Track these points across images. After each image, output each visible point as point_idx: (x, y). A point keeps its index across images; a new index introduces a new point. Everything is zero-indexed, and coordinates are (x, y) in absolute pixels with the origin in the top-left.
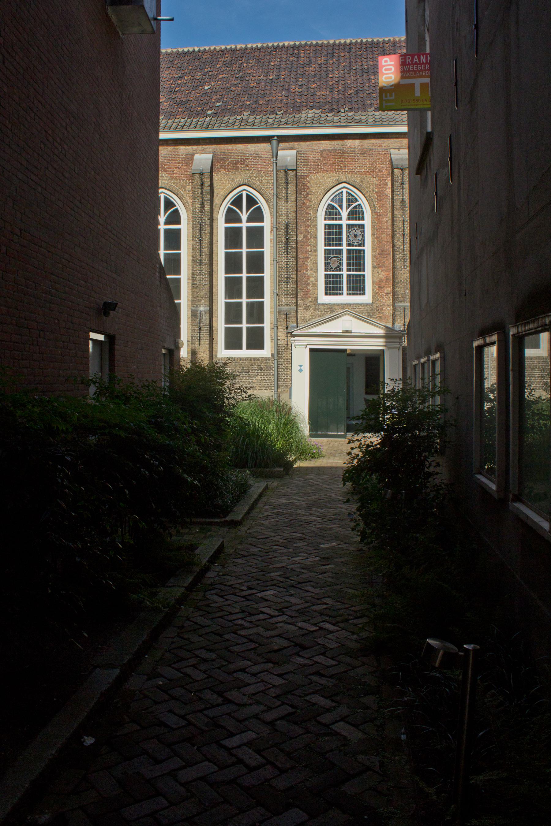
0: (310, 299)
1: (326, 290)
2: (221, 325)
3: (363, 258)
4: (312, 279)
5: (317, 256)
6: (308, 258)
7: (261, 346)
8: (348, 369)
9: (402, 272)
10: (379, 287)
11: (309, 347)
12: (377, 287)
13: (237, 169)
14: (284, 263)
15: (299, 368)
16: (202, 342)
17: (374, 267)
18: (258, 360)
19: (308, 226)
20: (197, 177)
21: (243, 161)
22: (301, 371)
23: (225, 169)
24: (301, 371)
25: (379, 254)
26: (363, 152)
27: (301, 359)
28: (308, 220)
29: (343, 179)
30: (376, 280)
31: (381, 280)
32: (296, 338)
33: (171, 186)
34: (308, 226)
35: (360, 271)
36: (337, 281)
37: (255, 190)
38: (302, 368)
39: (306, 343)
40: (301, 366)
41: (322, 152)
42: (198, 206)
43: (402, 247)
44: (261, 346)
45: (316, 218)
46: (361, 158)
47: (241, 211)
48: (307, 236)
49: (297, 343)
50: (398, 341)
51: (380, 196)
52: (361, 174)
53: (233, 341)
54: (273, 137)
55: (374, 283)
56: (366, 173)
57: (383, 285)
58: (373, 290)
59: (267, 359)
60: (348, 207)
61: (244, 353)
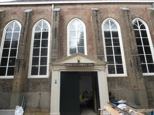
0: (64, 56)
1: (70, 53)
2: (30, 66)
3: (84, 49)
4: (65, 49)
5: (67, 41)
6: (63, 41)
7: (122, 72)
8: (70, 42)
9: (99, 44)
10: (90, 51)
11: (60, 71)
12: (89, 51)
13: (40, 14)
14: (54, 42)
15: (55, 81)
16: (19, 72)
17: (87, 44)
18: (44, 79)
19: (64, 31)
20: (25, 14)
21: (43, 12)
22: (56, 83)
23: (36, 14)
24: (56, 83)
25: (89, 40)
26: (82, 9)
27: (56, 77)
28: (64, 29)
29: (76, 16)
30: (88, 49)
31: (90, 49)
32: (54, 67)
33: (17, 19)
34: (64, 31)
35: (82, 46)
36: (74, 51)
37: (46, 20)
38: (56, 81)
39: (59, 69)
40: (56, 80)
41: (69, 9)
42: (24, 23)
43: (98, 35)
44: (122, 72)
45: (67, 29)
46: (81, 10)
47: (138, 25)
48: (64, 34)
49: (54, 69)
50: (104, 67)
51: (88, 22)
52: (82, 15)
53: (34, 72)
54: (53, 4)
55: (88, 50)
56: (83, 15)
57: (91, 50)
58: (87, 52)
59: (47, 79)
60: (43, 27)
61: (39, 76)
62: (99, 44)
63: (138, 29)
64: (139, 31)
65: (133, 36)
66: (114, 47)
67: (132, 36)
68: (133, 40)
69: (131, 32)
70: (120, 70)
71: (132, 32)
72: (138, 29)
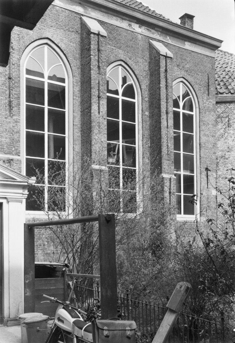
7: (133, 210)
44: (133, 210)
62: (9, 122)
63: (179, 108)
64: (117, 100)
65: (101, 113)
66: (180, 151)
67: (99, 113)
68: (99, 126)
69: (99, 103)
70: (57, 205)
71: (101, 102)
72: (179, 108)
